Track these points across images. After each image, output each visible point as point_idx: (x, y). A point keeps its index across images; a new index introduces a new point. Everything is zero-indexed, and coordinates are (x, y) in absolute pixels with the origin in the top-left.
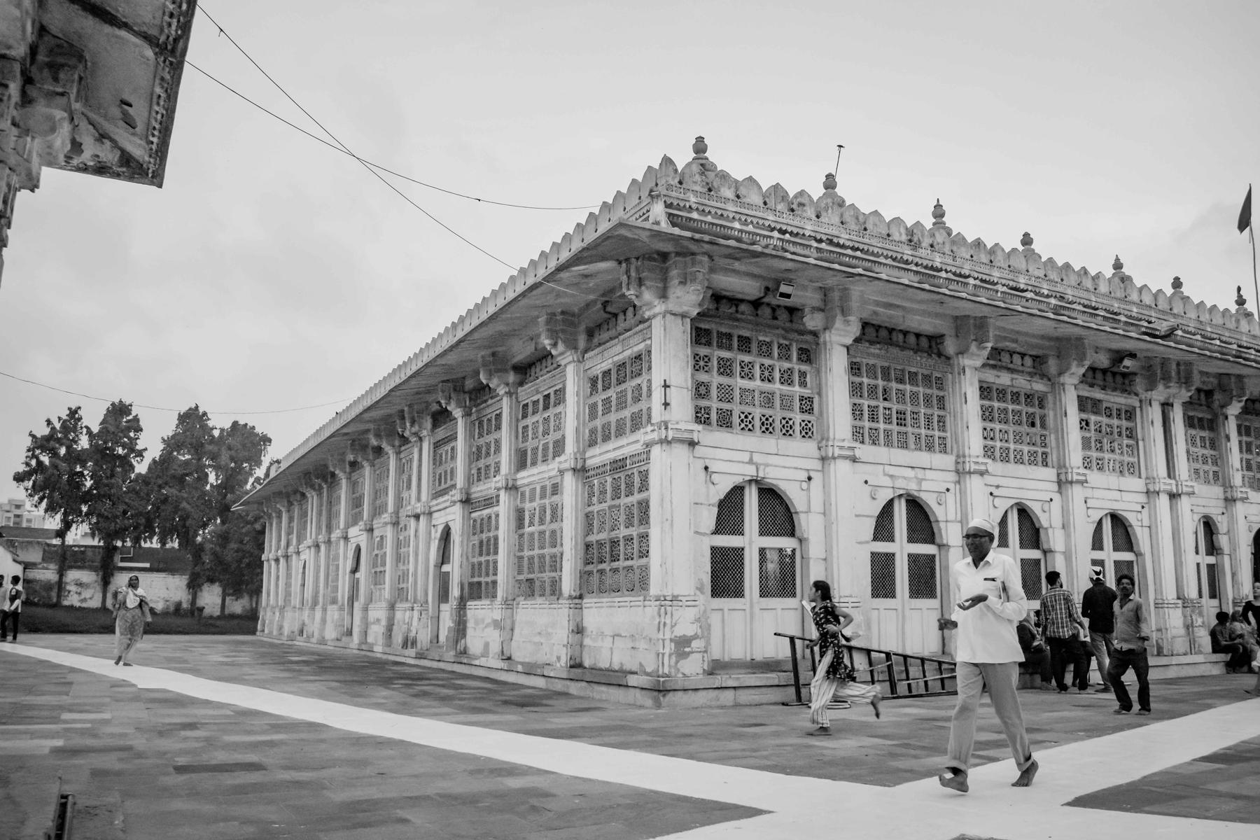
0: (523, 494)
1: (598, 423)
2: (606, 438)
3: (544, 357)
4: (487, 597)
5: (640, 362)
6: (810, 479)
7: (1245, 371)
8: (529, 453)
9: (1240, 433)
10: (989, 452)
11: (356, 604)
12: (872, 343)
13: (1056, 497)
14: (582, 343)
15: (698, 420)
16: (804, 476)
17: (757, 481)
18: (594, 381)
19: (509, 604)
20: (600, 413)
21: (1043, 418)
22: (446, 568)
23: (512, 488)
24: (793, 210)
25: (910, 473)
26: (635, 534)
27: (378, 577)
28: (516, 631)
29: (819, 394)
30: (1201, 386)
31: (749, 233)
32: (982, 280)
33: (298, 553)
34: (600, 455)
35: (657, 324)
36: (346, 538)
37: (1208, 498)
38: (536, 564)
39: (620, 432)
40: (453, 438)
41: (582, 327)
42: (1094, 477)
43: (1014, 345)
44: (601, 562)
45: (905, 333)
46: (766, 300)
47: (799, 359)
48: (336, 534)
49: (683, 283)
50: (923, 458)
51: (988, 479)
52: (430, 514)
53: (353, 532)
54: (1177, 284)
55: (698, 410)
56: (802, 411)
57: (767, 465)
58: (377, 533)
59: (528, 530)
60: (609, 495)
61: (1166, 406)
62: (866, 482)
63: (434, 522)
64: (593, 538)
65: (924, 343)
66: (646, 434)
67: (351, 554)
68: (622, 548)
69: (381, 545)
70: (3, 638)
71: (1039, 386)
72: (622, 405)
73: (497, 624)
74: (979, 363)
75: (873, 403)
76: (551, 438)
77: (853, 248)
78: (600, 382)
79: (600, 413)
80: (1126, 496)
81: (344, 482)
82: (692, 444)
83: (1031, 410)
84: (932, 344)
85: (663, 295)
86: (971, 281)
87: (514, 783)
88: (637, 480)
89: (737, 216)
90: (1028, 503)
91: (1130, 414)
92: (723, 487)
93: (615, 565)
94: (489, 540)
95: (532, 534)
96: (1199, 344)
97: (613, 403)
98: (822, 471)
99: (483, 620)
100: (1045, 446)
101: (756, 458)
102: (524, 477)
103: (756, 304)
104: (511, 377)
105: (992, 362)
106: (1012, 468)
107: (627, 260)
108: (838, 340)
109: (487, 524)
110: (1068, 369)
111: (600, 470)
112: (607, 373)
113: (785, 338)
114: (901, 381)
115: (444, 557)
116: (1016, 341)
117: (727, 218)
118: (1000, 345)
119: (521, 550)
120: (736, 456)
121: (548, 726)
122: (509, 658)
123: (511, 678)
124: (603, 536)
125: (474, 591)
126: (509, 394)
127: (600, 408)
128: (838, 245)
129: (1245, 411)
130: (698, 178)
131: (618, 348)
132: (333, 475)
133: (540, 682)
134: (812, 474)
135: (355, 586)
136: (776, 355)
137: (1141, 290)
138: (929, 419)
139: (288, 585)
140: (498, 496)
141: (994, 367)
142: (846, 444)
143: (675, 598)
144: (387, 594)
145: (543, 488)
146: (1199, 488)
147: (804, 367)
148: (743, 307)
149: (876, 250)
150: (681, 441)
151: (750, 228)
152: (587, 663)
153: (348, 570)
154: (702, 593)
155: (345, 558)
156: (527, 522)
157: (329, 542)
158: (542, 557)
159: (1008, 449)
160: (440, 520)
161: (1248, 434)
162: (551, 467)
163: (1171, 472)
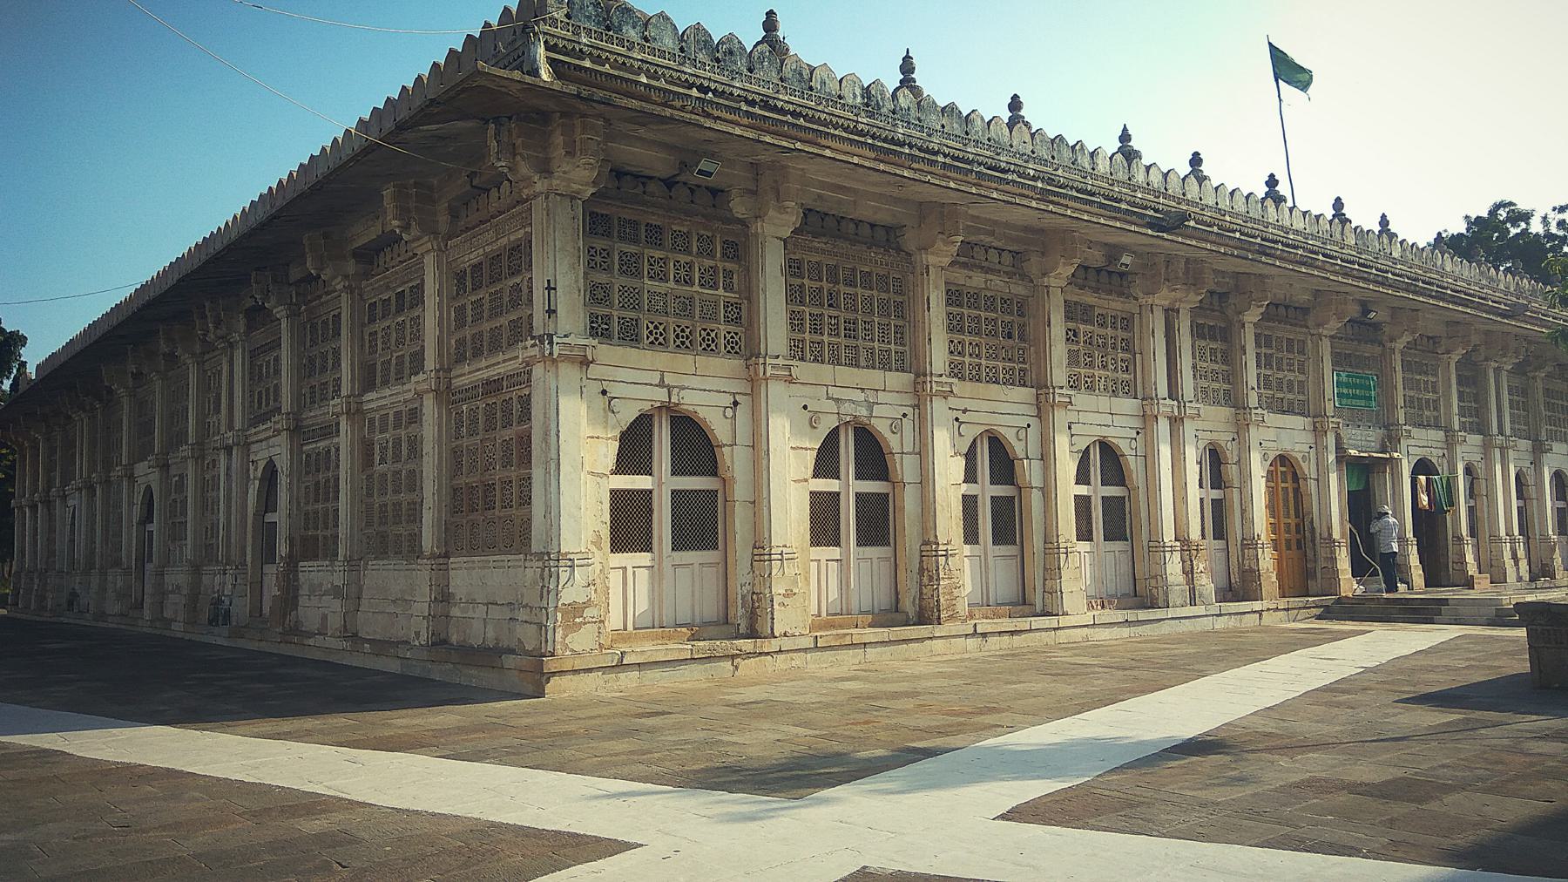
0: (372, 421)
1: (468, 332)
2: (477, 353)
3: (390, 241)
4: (325, 557)
5: (518, 257)
6: (736, 403)
7: (1266, 270)
8: (379, 367)
9: (1258, 345)
10: (956, 371)
11: (148, 566)
12: (816, 235)
13: (1034, 422)
14: (443, 221)
15: (594, 332)
16: (729, 400)
17: (668, 408)
18: (460, 277)
19: (353, 563)
20: (469, 319)
21: (1022, 327)
22: (270, 517)
23: (356, 412)
24: (718, 60)
25: (859, 396)
26: (514, 475)
27: (176, 532)
28: (364, 602)
29: (749, 299)
30: (1213, 287)
31: (660, 89)
32: (953, 158)
33: (64, 498)
34: (469, 375)
35: (538, 205)
36: (131, 478)
37: (1210, 422)
38: (390, 514)
39: (495, 347)
40: (277, 344)
41: (443, 205)
42: (1081, 399)
43: (989, 239)
44: (474, 510)
45: (858, 223)
46: (682, 178)
47: (724, 255)
48: (118, 471)
49: (570, 153)
50: (875, 377)
51: (952, 402)
52: (248, 445)
53: (141, 468)
54: (1196, 160)
55: (593, 318)
56: (728, 321)
58: (173, 471)
59: (379, 468)
60: (481, 426)
61: (1170, 313)
62: (805, 407)
63: (252, 457)
64: (462, 480)
65: (880, 234)
66: (528, 350)
67: (138, 499)
68: (498, 493)
69: (181, 486)
70: (1566, 335)
71: (1019, 289)
72: (496, 312)
73: (336, 592)
74: (946, 261)
75: (816, 311)
76: (407, 351)
77: (794, 114)
78: (469, 278)
79: (469, 319)
80: (1118, 420)
81: (125, 400)
82: (585, 363)
83: (1008, 318)
84: (887, 237)
85: (546, 170)
86: (940, 159)
87: (312, 826)
88: (516, 406)
89: (645, 66)
90: (1001, 430)
91: (1127, 322)
92: (628, 414)
93: (489, 514)
94: (328, 481)
95: (384, 475)
96: (1213, 238)
97: (486, 306)
98: (751, 395)
100: (1024, 362)
102: (373, 400)
103: (669, 183)
104: (351, 267)
105: (963, 259)
106: (981, 388)
107: (496, 120)
108: (774, 231)
109: (327, 460)
110: (1054, 268)
111: (470, 393)
112: (477, 267)
113: (705, 229)
114: (852, 284)
116: (992, 233)
117: (631, 70)
118: (972, 239)
119: (370, 495)
120: (641, 378)
121: (387, 733)
122: (355, 635)
123: (356, 661)
124: (473, 480)
125: (312, 546)
126: (350, 290)
127: (469, 312)
128: (775, 109)
129: (1266, 317)
132: (110, 391)
133: (393, 666)
135: (145, 542)
136: (695, 249)
137: (1148, 168)
138: (884, 329)
139: (51, 541)
140: (338, 424)
141: (964, 265)
142: (780, 361)
144: (188, 552)
145: (398, 414)
146: (1208, 410)
147: (729, 266)
148: (651, 187)
149: (823, 116)
150: (569, 359)
151: (662, 84)
152: (454, 639)
154: (600, 549)
155: (131, 504)
156: (377, 458)
157: (108, 482)
158: (397, 505)
159: (979, 365)
160: (261, 455)
161: (1268, 346)
162: (406, 387)
163: (1173, 392)
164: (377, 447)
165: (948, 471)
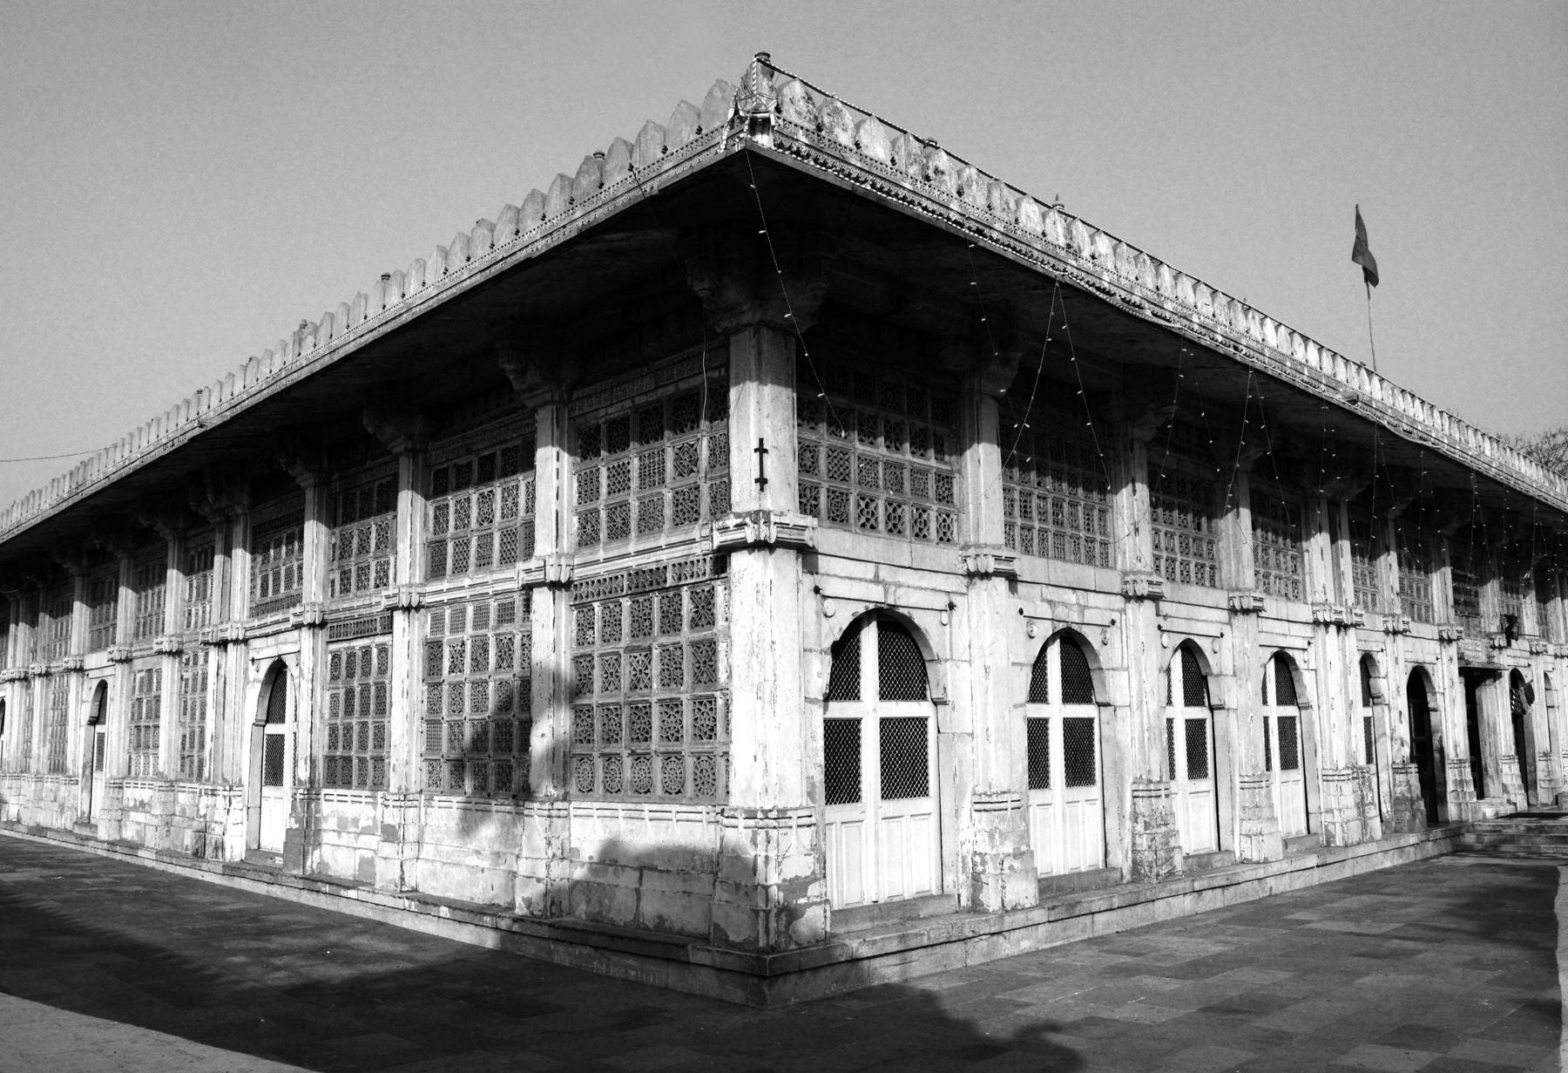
6: (952, 606)
16: (942, 602)
57: (899, 585)
62: (1021, 612)
99: (356, 821)
101: (884, 573)
115: (274, 707)
120: (860, 569)
130: (802, 105)
131: (648, 383)
134: (956, 599)
143: (783, 814)
153: (85, 718)
156: (446, 664)
164: (446, 651)
165: (655, 686)
